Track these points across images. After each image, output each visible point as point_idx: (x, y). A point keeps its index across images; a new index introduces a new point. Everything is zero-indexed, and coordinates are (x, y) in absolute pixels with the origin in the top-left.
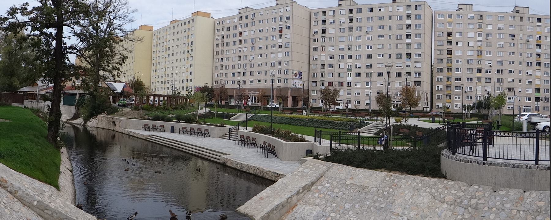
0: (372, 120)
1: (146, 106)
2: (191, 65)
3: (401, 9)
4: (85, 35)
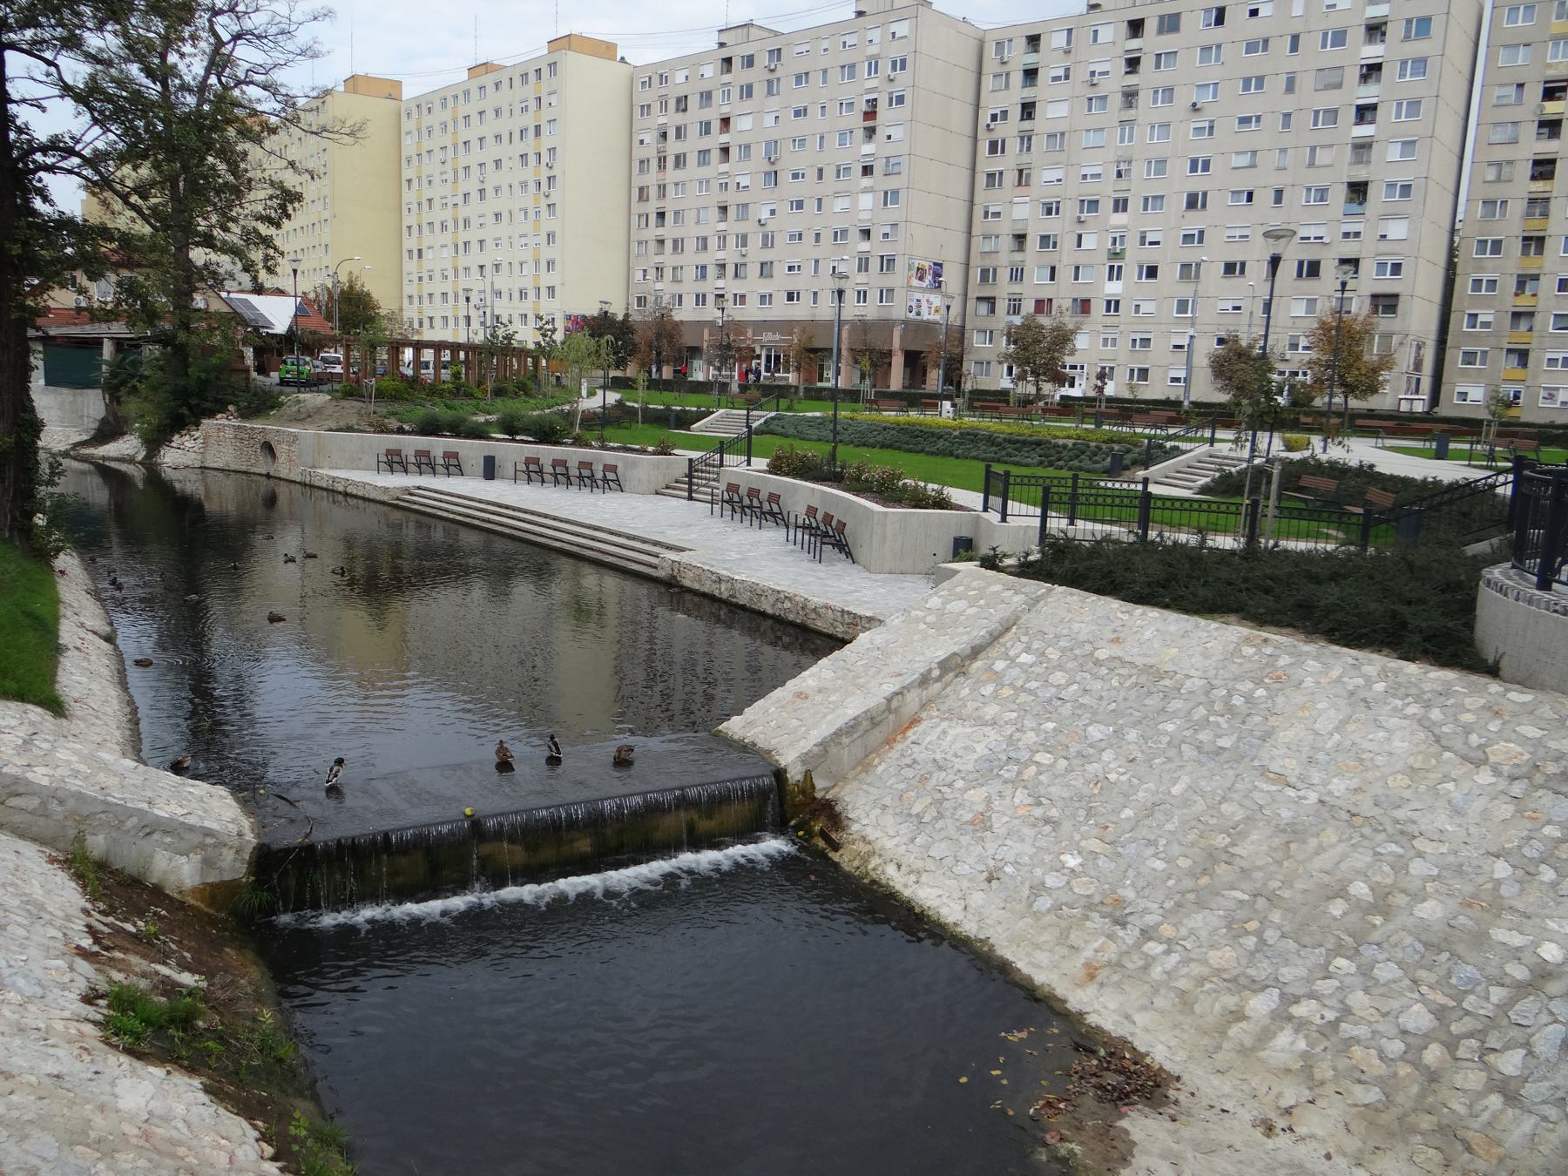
0: (1190, 440)
1: (387, 383)
2: (550, 237)
4: (109, 99)
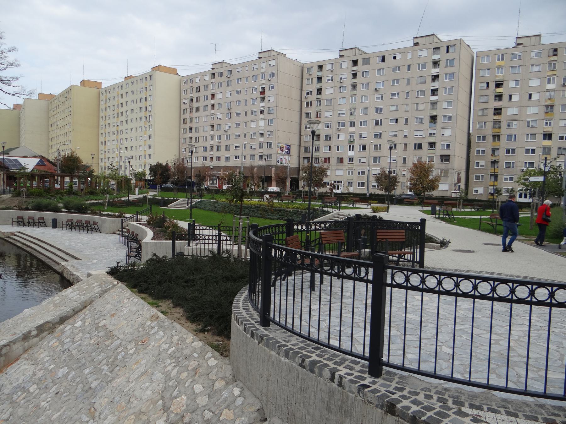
2: (150, 136)
3: (425, 53)
